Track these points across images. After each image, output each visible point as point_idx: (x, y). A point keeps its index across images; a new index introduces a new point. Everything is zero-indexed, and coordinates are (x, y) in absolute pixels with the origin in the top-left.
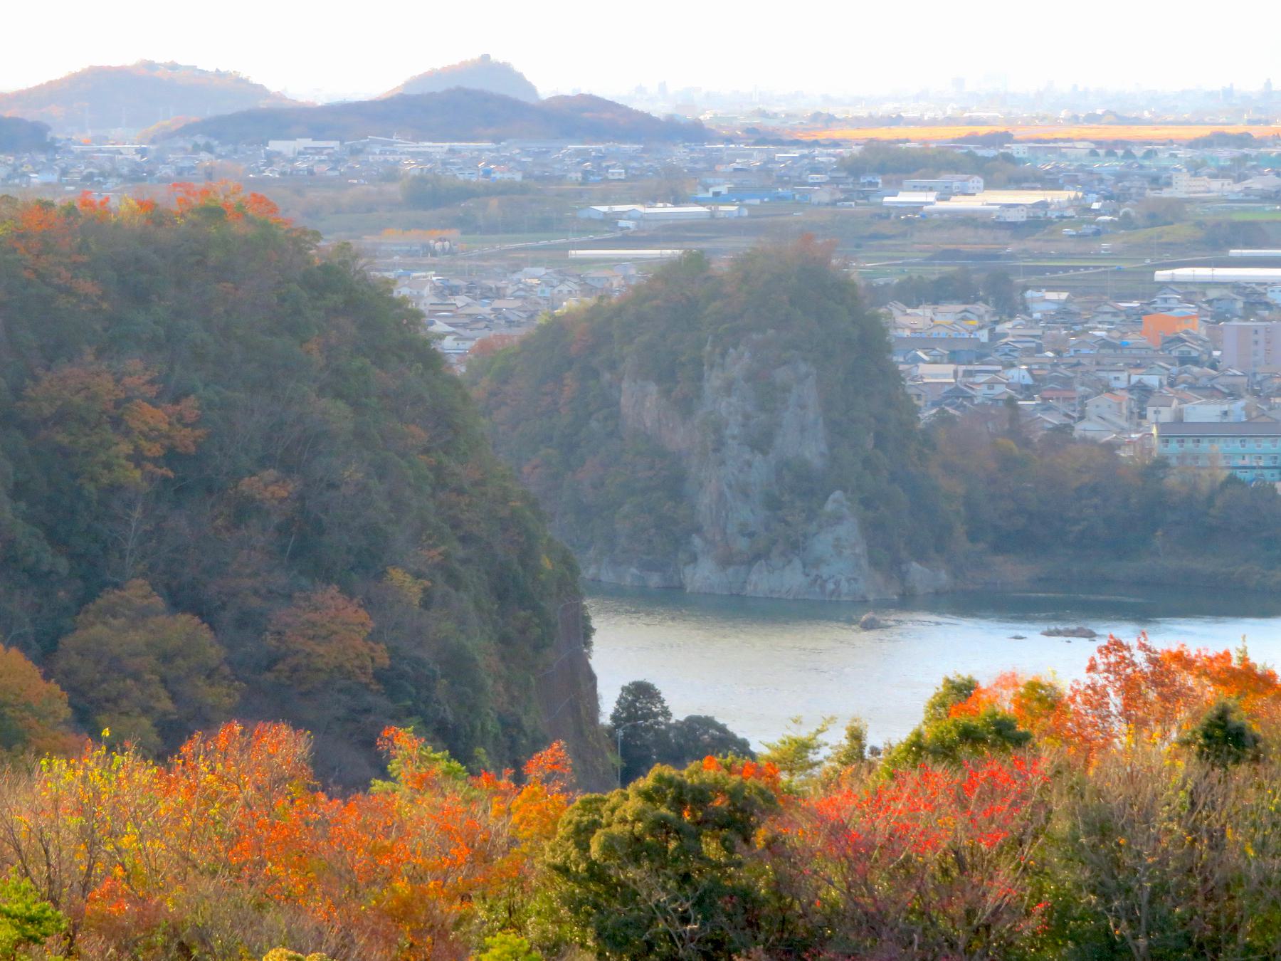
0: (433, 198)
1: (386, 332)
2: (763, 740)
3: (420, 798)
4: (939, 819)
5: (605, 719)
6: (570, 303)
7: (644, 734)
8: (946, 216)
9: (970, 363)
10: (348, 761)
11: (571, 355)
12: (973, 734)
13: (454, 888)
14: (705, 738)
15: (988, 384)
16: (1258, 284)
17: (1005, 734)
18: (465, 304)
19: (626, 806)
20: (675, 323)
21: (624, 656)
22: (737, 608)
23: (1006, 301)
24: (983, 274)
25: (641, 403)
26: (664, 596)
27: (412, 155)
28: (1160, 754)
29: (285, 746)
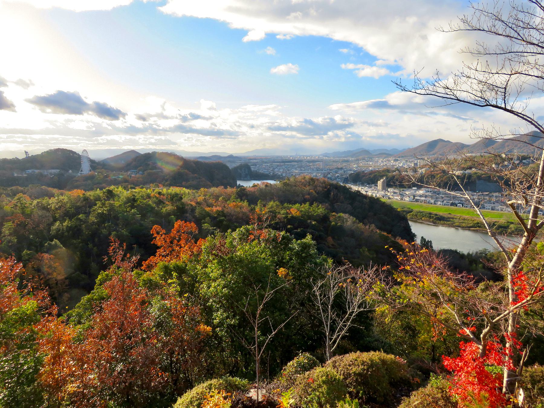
0: (229, 161)
1: (227, 167)
2: (245, 186)
3: (229, 190)
4: (253, 189)
5: (341, 50)
6: (236, 166)
7: (239, 186)
8: (288, 37)
9: (513, 290)
10: (226, 188)
11: (236, 169)
12: (255, 186)
13: (162, 278)
14: (242, 186)
15: (255, 169)
16: (309, 162)
17: (256, 186)
18: (231, 166)
19: (239, 189)
20: (241, 167)
21: (238, 182)
22: (244, 180)
23: (256, 165)
24: (255, 165)
25: (239, 171)
26: (240, 180)
27: (228, 159)
28: (264, 186)
29: (222, 187)
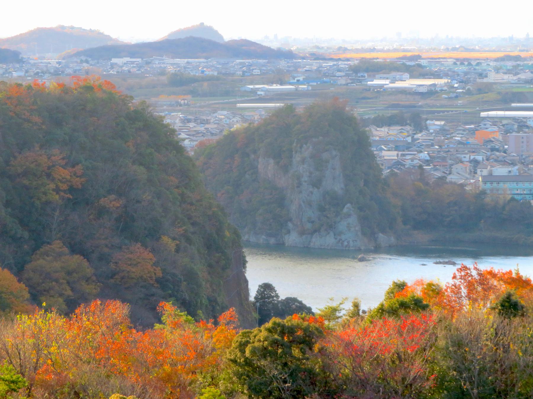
0: (180, 82)
1: (161, 138)
2: (317, 307)
3: (175, 331)
4: (391, 340)
5: (252, 299)
6: (237, 126)
7: (268, 305)
8: (394, 90)
9: (404, 151)
10: (145, 316)
11: (238, 148)
12: (405, 305)
13: (189, 369)
14: (293, 306)
15: (411, 160)
16: (523, 118)
17: (418, 305)
18: (194, 126)
19: (260, 335)
20: (281, 134)
21: (260, 273)
22: (307, 252)
23: (419, 125)
24: (409, 114)
25: (267, 167)
26: (276, 248)
27: (172, 64)
28: (483, 313)
29: (119, 310)
